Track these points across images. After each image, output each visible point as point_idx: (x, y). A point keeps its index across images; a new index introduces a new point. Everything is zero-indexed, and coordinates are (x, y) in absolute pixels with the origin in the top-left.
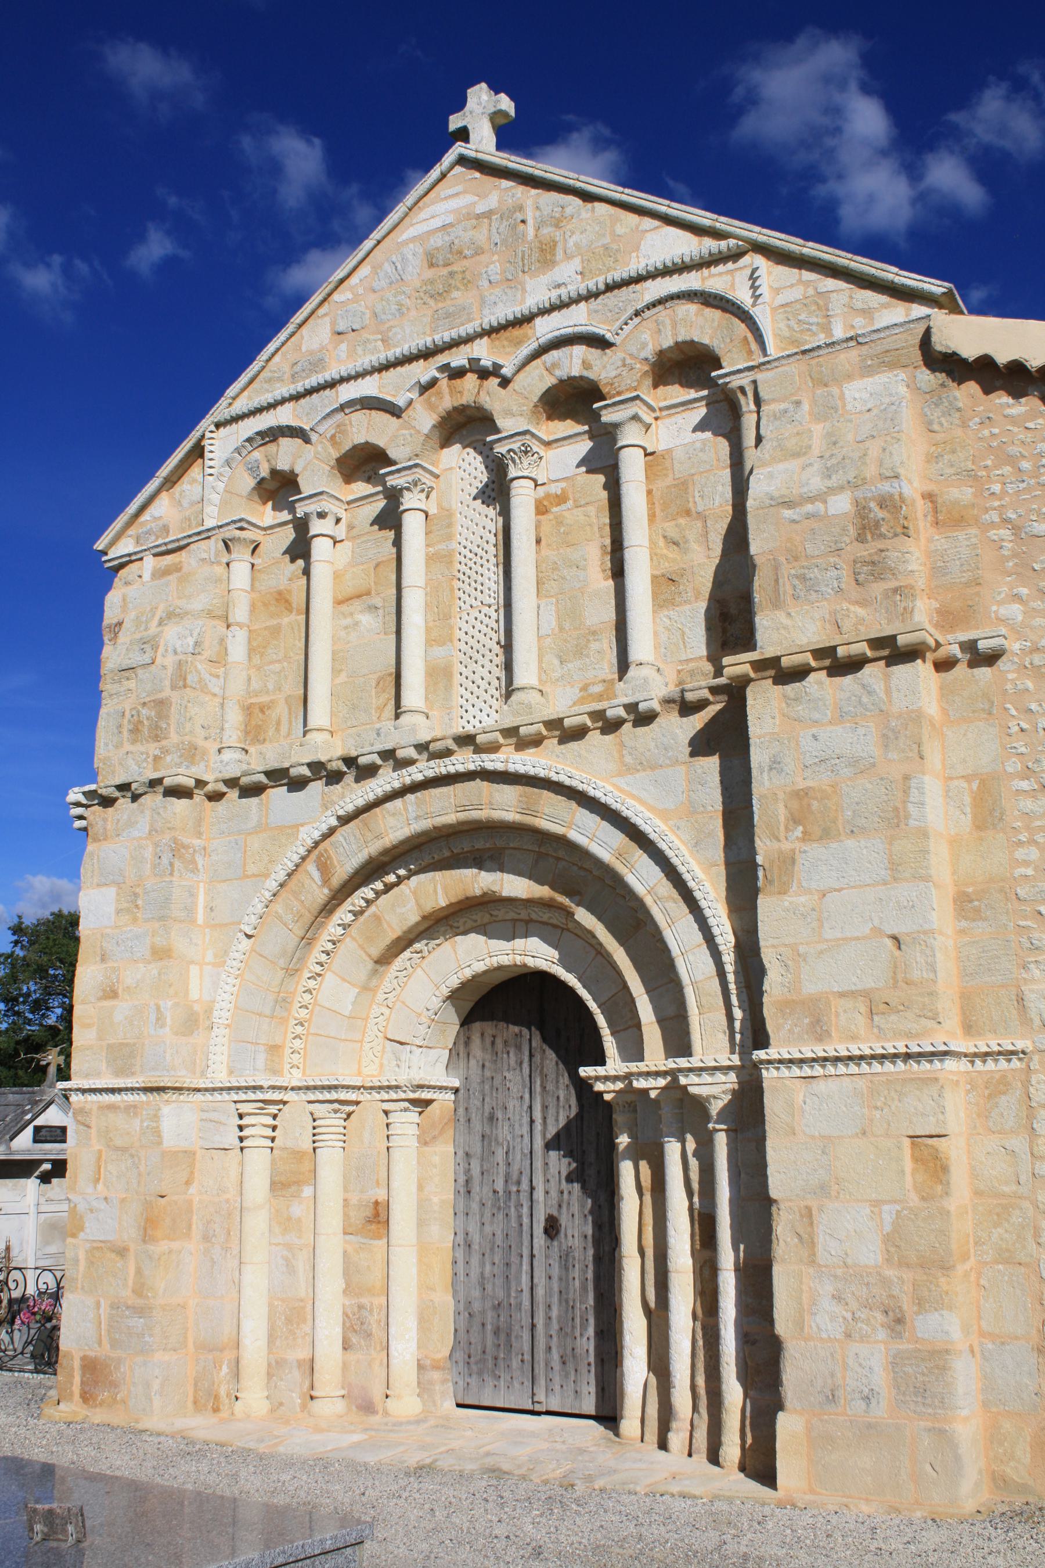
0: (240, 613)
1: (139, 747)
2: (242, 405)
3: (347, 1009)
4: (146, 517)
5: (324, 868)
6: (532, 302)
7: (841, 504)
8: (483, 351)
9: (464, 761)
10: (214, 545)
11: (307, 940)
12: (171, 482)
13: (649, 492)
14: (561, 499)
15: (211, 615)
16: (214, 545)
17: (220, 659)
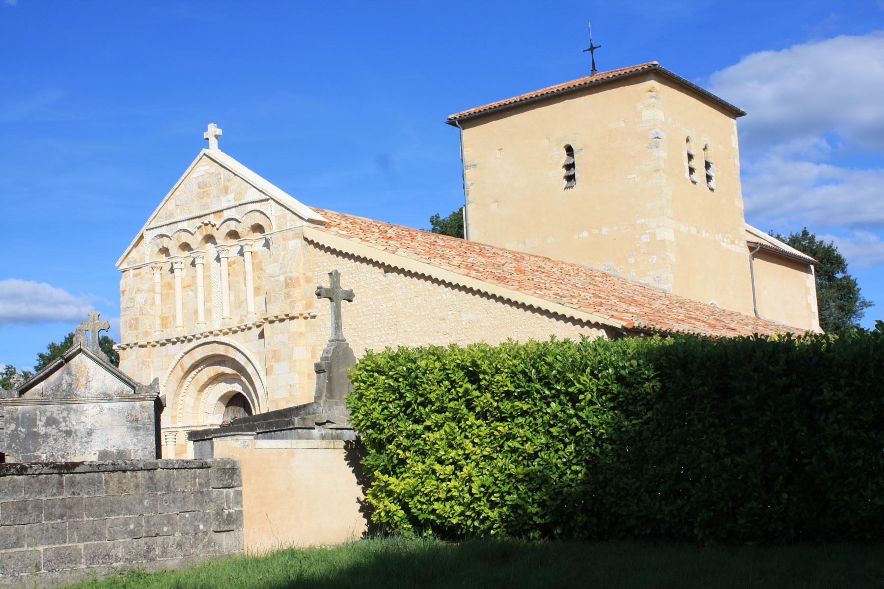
0: (158, 289)
1: (132, 332)
2: (153, 225)
3: (192, 405)
4: (129, 256)
5: (182, 366)
6: (224, 205)
7: (282, 278)
8: (212, 219)
9: (211, 338)
10: (148, 269)
11: (180, 386)
12: (136, 245)
13: (253, 263)
14: (234, 263)
15: (149, 291)
16: (148, 269)
17: (153, 303)
